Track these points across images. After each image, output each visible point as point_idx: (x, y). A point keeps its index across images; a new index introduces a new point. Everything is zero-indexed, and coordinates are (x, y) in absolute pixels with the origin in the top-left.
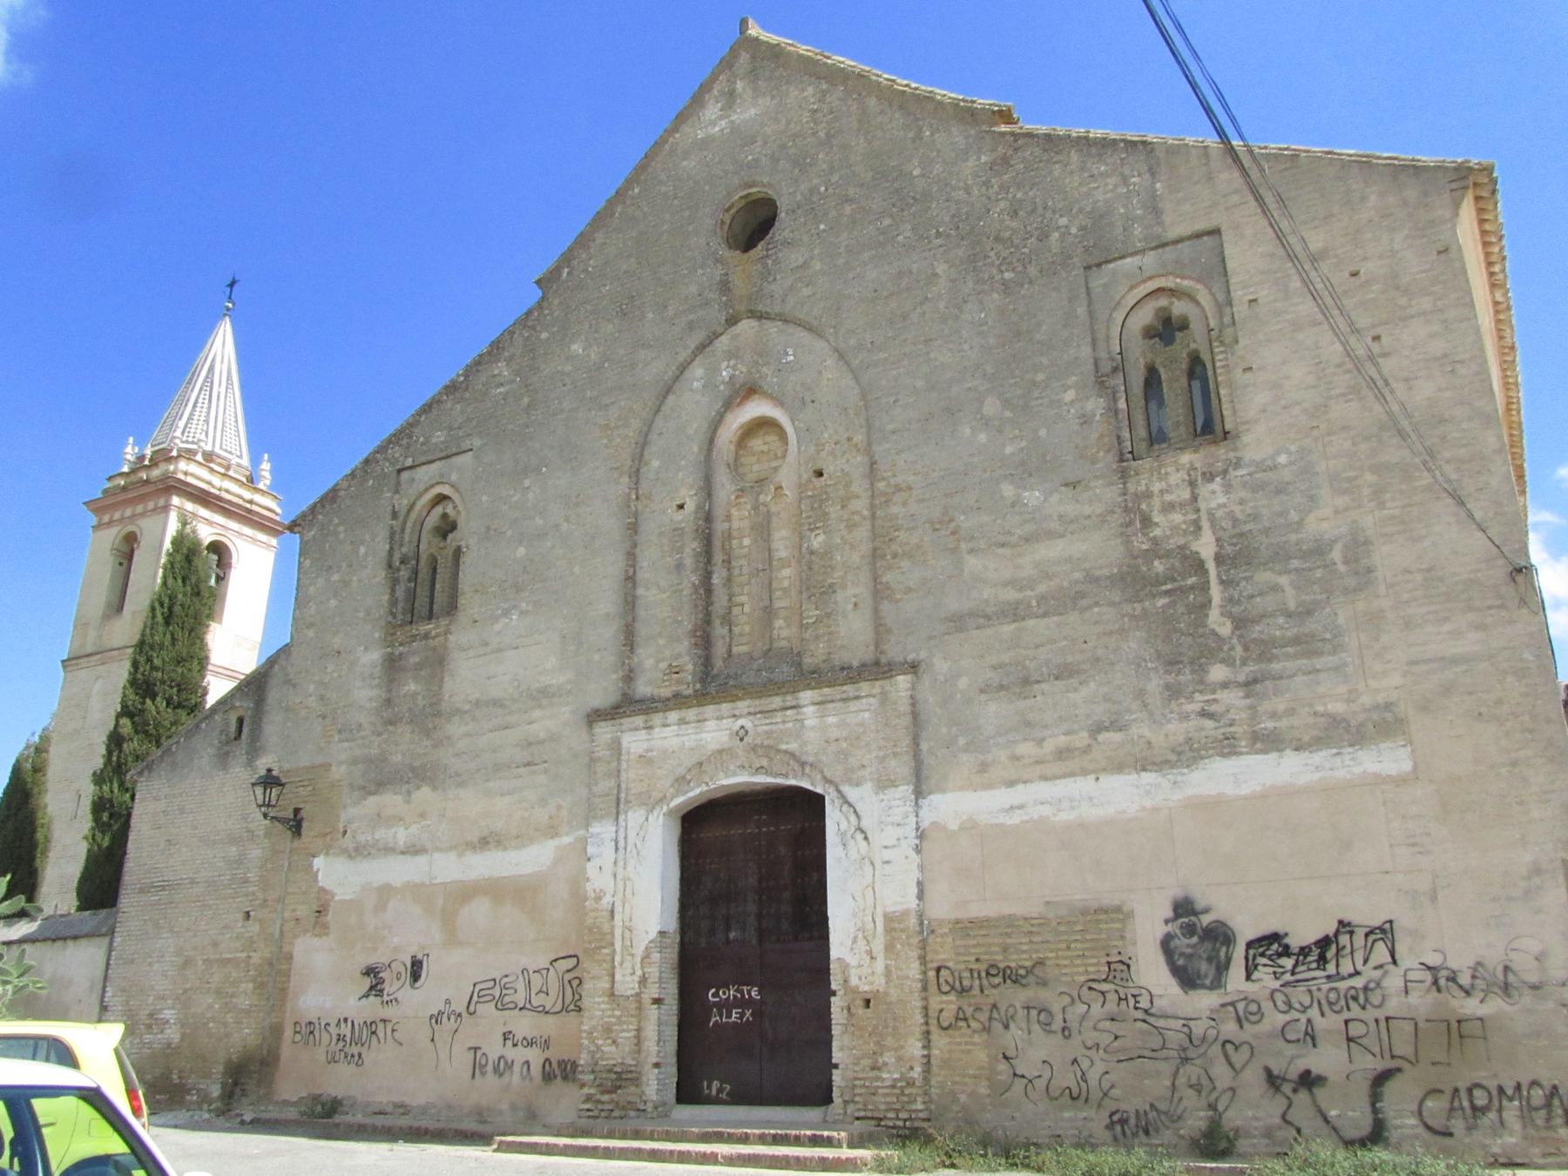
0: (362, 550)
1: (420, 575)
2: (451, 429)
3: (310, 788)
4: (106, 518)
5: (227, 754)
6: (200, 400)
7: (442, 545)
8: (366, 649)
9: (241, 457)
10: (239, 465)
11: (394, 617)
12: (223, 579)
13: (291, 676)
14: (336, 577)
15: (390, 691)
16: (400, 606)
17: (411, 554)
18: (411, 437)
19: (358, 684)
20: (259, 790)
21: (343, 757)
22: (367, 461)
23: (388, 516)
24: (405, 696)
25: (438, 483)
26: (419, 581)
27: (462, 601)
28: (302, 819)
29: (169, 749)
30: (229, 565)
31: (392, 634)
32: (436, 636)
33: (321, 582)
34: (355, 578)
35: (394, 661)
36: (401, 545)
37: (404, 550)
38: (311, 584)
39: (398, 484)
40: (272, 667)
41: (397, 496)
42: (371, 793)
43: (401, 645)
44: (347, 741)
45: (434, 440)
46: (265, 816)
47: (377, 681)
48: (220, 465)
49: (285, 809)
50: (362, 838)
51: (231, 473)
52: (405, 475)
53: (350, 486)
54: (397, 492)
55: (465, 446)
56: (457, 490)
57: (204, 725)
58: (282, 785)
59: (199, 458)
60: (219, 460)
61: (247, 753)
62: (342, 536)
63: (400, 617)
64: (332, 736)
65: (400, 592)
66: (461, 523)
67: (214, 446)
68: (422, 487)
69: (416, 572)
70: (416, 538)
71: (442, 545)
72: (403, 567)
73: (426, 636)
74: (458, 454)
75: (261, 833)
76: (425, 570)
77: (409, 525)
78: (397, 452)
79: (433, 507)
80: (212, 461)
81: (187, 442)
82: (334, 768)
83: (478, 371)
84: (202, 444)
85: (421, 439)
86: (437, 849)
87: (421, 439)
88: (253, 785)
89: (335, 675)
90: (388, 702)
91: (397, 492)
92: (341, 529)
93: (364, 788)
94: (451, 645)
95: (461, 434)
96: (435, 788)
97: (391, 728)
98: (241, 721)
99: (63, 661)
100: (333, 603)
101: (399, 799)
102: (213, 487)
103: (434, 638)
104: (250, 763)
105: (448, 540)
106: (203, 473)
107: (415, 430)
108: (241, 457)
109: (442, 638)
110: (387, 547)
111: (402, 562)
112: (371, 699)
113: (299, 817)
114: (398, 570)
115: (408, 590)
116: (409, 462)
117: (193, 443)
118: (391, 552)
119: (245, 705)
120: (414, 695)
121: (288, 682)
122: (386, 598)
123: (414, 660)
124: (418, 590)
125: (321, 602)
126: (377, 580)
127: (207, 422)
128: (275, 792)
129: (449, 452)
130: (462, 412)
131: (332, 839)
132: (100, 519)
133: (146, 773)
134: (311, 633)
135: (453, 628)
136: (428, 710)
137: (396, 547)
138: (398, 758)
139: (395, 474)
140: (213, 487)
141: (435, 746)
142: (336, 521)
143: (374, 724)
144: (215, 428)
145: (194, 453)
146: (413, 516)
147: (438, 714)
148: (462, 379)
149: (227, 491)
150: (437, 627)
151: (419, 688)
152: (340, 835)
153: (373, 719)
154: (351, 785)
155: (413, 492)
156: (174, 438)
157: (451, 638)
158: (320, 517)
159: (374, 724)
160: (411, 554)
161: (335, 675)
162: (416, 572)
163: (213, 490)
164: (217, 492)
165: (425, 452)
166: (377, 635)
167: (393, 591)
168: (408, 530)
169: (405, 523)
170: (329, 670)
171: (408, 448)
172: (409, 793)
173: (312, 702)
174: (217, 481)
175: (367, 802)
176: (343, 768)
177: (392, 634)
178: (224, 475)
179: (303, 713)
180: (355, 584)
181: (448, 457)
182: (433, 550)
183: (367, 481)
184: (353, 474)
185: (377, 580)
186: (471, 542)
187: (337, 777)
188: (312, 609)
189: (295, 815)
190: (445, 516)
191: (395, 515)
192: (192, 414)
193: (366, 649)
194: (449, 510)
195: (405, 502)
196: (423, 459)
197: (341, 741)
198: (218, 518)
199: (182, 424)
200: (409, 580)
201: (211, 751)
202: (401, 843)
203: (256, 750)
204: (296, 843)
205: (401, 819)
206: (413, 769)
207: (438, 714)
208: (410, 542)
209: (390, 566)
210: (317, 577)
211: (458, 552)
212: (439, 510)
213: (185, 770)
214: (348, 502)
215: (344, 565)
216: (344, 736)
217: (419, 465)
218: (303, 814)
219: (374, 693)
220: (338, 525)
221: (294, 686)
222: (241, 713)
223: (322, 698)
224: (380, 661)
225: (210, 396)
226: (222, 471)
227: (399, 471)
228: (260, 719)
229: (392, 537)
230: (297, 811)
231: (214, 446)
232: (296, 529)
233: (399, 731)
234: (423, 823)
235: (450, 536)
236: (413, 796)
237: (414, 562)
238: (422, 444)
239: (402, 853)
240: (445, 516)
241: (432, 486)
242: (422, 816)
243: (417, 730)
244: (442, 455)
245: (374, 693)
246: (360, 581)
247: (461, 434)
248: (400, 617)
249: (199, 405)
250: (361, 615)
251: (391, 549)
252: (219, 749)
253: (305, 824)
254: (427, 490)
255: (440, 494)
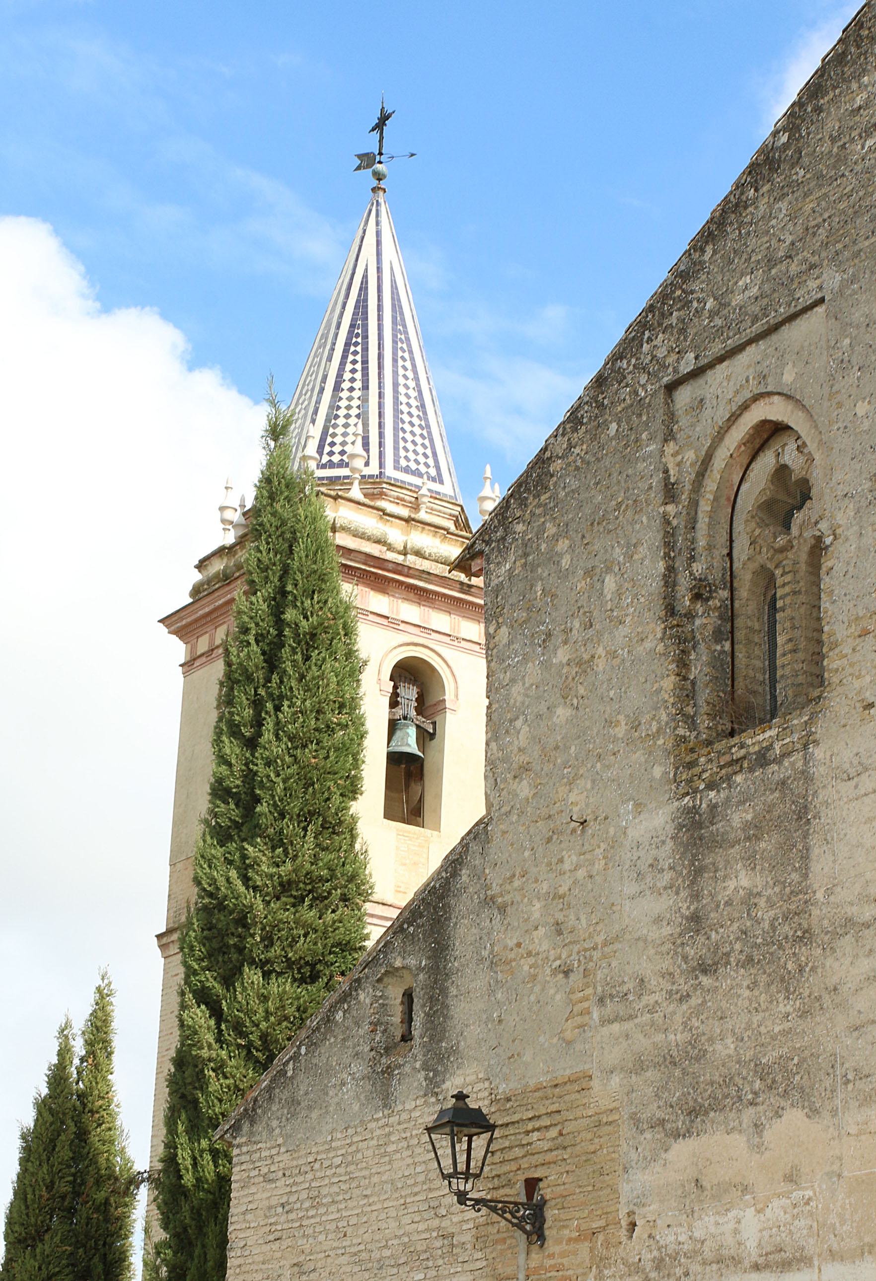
0: (610, 583)
1: (739, 622)
2: (771, 262)
3: (553, 1133)
4: (203, 645)
5: (388, 1071)
6: (347, 376)
7: (781, 541)
8: (639, 807)
9: (439, 479)
10: (436, 496)
11: (691, 722)
12: (432, 736)
13: (495, 889)
14: (562, 655)
15: (696, 896)
16: (704, 695)
17: (715, 576)
18: (687, 304)
19: (631, 888)
20: (443, 1142)
21: (614, 1055)
22: (600, 382)
23: (655, 495)
24: (728, 903)
25: (756, 398)
26: (740, 635)
27: (832, 663)
28: (544, 1202)
29: (282, 1073)
30: (440, 707)
31: (691, 765)
32: (785, 755)
33: (533, 671)
34: (600, 651)
35: (700, 825)
36: (692, 559)
37: (698, 568)
38: (513, 681)
39: (671, 417)
40: (455, 874)
41: (670, 448)
42: (677, 1135)
43: (711, 786)
44: (617, 1019)
45: (737, 299)
46: (462, 1197)
47: (668, 876)
48: (400, 501)
49: (509, 1184)
50: (668, 1238)
51: (422, 515)
52: (684, 396)
53: (570, 446)
54: (669, 436)
55: (806, 294)
56: (799, 404)
57: (339, 1016)
58: (491, 1128)
59: (356, 492)
60: (395, 493)
61: (426, 1067)
62: (565, 562)
63: (704, 722)
64: (587, 1012)
65: (699, 668)
66: (817, 477)
67: (381, 465)
68: (723, 414)
69: (730, 615)
70: (723, 537)
71: (781, 541)
72: (699, 608)
73: (763, 759)
74: (792, 318)
75: (467, 1238)
76: (752, 608)
77: (705, 507)
78: (662, 344)
79: (753, 458)
80: (381, 495)
81: (331, 465)
82: (595, 1084)
83: (818, 110)
84: (359, 463)
85: (710, 304)
86: (833, 1255)
87: (710, 304)
88: (429, 1130)
89: (581, 873)
90: (696, 920)
91: (669, 436)
92: (563, 545)
93: (662, 1122)
94: (819, 771)
95: (794, 268)
96: (813, 1112)
97: (706, 981)
98: (408, 997)
99: (159, 937)
100: (562, 713)
101: (739, 1141)
102: (390, 548)
103: (778, 761)
104: (433, 1086)
105: (795, 531)
106: (368, 522)
107: (696, 286)
108: (439, 479)
109: (797, 757)
110: (661, 566)
111: (697, 597)
112: (658, 920)
113: (537, 1198)
114: (690, 616)
115: (716, 661)
116: (688, 363)
117: (342, 464)
118: (670, 578)
119: (412, 962)
120: (750, 899)
121: (489, 901)
122: (669, 683)
123: (739, 817)
124: (740, 655)
125: (539, 716)
126: (648, 645)
127: (363, 416)
128: (480, 1142)
129: (772, 318)
130: (792, 217)
131: (607, 1244)
132: (193, 649)
133: (246, 1127)
134: (524, 789)
135: (819, 730)
136: (786, 929)
137: (679, 564)
138: (725, 1048)
139: (661, 395)
140: (390, 548)
141: (804, 1014)
142: (551, 529)
143: (669, 975)
144: (381, 425)
145: (345, 481)
146: (711, 485)
147: (805, 937)
148: (784, 138)
149: (418, 553)
150: (786, 730)
151: (759, 881)
152: (623, 1232)
153: (666, 964)
154: (635, 1119)
155: (705, 427)
156: (304, 458)
157: (818, 753)
158: (520, 528)
159: (669, 975)
160: (715, 576)
161: (581, 873)
162: (730, 615)
163: (390, 556)
164: (400, 559)
165: (720, 330)
166: (658, 771)
167: (683, 664)
168: (703, 521)
169: (694, 504)
170: (567, 866)
171: (682, 331)
172: (758, 1127)
173: (541, 942)
174: (396, 534)
175: (671, 1155)
176: (616, 1080)
177: (691, 765)
178: (408, 520)
179: (526, 966)
180: (601, 665)
181: (775, 328)
182: (764, 557)
183: (606, 425)
184: (574, 419)
185: (648, 645)
186: (841, 518)
187: (605, 1103)
188: (523, 734)
189: (530, 1195)
190: (782, 472)
191: (670, 492)
192: (334, 406)
193: (639, 807)
194: (790, 456)
195: (690, 456)
196: (717, 348)
197: (606, 1021)
198: (410, 611)
199: (316, 431)
200: (718, 636)
201: (359, 1068)
202: (751, 1245)
203: (441, 1058)
204: (536, 1257)
205: (745, 1189)
206: (762, 1072)
207: (805, 937)
208: (710, 548)
209: (671, 610)
210: (526, 659)
211: (818, 549)
212: (767, 462)
213: (315, 1115)
214: (572, 482)
215: (577, 624)
216: (610, 1007)
217: (711, 366)
218: (545, 1190)
219: (663, 904)
220: (556, 538)
221: (502, 909)
222: (408, 981)
223: (558, 928)
224: (670, 829)
225: (365, 362)
226: (405, 512)
227: (671, 388)
228: (444, 991)
229: (669, 543)
230: (532, 1185)
231: (381, 465)
232: (476, 565)
233: (726, 984)
234: (797, 1195)
235: (799, 517)
236: (767, 1134)
237: (725, 594)
238: (713, 314)
239: (756, 1267)
240: (782, 472)
241: (745, 407)
242: (791, 1178)
243: (763, 979)
244: (758, 328)
245: (663, 904)
246: (613, 655)
247: (794, 268)
248: (704, 722)
249: (346, 385)
250: (621, 731)
251: (671, 569)
252: (374, 1062)
253: (550, 1214)
254: (734, 418)
255: (764, 422)
